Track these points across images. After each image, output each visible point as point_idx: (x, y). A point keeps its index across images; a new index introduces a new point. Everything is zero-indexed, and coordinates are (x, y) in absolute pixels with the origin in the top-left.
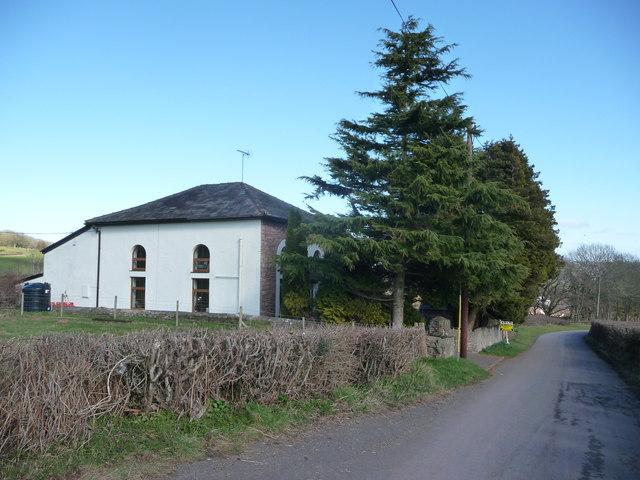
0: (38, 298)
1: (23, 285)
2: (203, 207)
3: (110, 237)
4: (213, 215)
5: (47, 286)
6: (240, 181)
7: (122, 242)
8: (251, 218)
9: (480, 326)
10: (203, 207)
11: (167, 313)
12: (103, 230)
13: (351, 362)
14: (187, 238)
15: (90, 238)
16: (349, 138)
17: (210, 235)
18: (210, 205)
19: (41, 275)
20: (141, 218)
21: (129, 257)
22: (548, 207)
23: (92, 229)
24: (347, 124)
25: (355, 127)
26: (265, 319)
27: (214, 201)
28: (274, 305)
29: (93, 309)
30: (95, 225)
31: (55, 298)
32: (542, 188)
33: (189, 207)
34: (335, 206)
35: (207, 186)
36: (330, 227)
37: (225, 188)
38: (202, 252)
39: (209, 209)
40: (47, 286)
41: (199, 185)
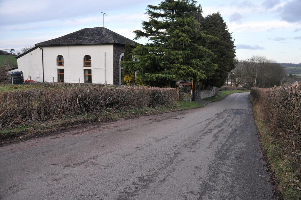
0: (19, 78)
1: (10, 72)
2: (87, 39)
3: (48, 51)
4: (92, 42)
5: (22, 73)
6: (103, 27)
7: (52, 53)
8: (109, 44)
9: (205, 89)
10: (87, 39)
11: (74, 84)
12: (44, 49)
13: (149, 99)
14: (82, 51)
15: (38, 50)
16: (150, 12)
17: (94, 51)
18: (90, 38)
19: (17, 68)
20: (60, 43)
21: (55, 61)
22: (208, 16)
23: (39, 48)
24: (150, 7)
25: (155, 8)
26: (115, 85)
27: (92, 36)
28: (119, 78)
29: (42, 83)
30: (41, 46)
31: (26, 78)
32: (229, 32)
33: (81, 39)
34: (144, 41)
35: (88, 29)
36: (144, 49)
37: (96, 30)
38: (87, 58)
39: (90, 40)
40: (22, 73)
41: (84, 28)
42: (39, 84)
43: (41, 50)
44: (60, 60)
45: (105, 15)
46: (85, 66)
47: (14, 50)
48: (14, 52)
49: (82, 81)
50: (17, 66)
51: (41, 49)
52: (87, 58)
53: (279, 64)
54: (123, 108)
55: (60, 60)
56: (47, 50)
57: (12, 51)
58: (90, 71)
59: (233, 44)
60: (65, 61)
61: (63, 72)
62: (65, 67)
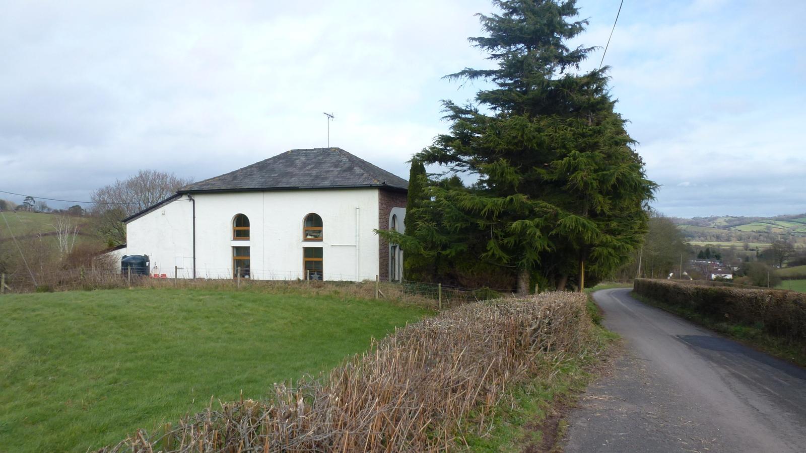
42: (186, 285)
43: (192, 202)
44: (241, 225)
45: (331, 118)
46: (234, 239)
47: (32, 198)
48: (32, 203)
49: (302, 278)
50: (124, 239)
51: (191, 199)
52: (313, 223)
53: (668, 220)
54: (213, 344)
55: (241, 225)
56: (202, 202)
57: (29, 202)
58: (319, 252)
59: (641, 174)
60: (254, 229)
61: (248, 255)
62: (253, 243)
